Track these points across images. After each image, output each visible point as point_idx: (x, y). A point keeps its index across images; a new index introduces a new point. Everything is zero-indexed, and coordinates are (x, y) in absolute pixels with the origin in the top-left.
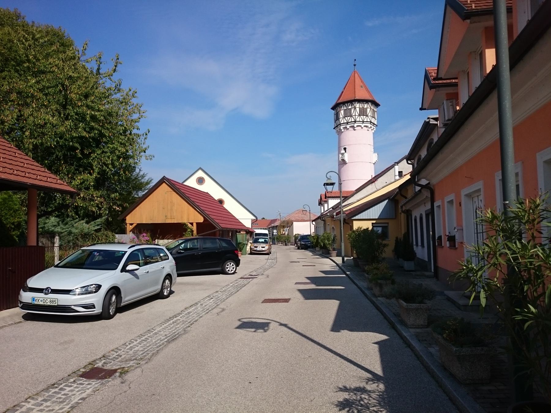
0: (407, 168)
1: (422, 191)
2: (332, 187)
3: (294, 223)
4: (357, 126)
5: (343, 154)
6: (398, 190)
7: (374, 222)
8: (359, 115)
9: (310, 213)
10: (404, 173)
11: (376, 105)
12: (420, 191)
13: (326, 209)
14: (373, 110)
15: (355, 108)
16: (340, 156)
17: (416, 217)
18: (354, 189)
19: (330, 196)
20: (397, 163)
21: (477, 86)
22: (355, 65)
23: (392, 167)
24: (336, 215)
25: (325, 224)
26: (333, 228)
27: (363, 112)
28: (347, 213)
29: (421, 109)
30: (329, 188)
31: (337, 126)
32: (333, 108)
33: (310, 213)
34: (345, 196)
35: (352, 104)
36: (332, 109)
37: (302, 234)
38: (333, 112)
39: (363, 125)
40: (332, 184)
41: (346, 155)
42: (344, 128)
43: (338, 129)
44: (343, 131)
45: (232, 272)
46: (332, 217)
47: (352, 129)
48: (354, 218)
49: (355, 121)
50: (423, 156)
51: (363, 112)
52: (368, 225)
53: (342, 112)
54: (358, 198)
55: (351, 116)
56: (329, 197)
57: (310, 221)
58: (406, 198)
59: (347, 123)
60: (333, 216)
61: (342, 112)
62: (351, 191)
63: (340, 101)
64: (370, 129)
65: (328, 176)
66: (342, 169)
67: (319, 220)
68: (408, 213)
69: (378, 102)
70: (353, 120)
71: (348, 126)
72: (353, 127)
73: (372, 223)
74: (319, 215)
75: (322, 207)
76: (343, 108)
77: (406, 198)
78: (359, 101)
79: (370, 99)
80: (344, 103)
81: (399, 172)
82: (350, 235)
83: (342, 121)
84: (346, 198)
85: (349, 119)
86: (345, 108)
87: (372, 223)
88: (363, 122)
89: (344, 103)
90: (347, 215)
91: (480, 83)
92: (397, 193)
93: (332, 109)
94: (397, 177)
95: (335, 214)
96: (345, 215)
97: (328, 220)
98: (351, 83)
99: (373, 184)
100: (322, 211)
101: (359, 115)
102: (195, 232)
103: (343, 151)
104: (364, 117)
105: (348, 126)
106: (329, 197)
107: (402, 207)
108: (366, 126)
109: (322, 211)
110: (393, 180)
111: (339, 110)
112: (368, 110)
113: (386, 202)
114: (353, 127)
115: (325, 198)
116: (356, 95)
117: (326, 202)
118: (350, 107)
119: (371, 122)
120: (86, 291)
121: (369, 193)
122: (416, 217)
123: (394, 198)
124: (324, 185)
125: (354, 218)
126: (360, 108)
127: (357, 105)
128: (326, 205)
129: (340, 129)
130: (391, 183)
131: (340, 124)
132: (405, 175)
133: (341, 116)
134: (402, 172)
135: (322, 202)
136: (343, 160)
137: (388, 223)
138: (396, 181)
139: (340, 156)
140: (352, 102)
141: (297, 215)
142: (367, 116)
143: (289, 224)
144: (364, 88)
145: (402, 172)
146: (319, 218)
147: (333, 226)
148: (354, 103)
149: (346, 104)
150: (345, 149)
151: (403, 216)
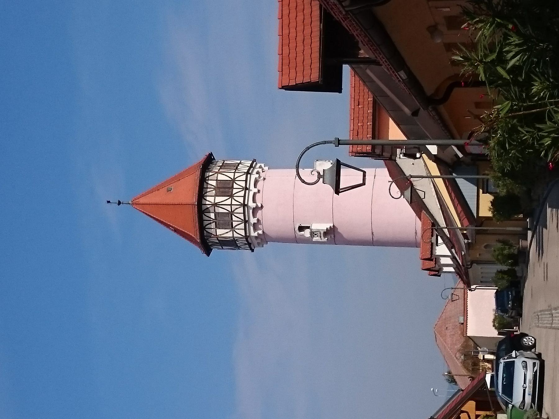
3: (469, 335)
4: (254, 201)
5: (313, 234)
7: (481, 191)
8: (231, 196)
11: (209, 161)
14: (221, 167)
15: (215, 205)
16: (316, 239)
19: (429, 253)
22: (119, 203)
24: (468, 239)
25: (479, 262)
26: (486, 247)
27: (226, 189)
31: (250, 244)
32: (208, 251)
35: (207, 210)
36: (208, 254)
37: (494, 306)
38: (215, 251)
39: (253, 190)
42: (255, 230)
43: (255, 242)
44: (260, 232)
45: (533, 339)
47: (259, 214)
49: (244, 205)
51: (226, 189)
52: (486, 200)
53: (220, 232)
55: (232, 213)
59: (246, 222)
60: (468, 243)
61: (220, 232)
64: (262, 175)
66: (345, 236)
69: (201, 157)
70: (241, 210)
71: (253, 220)
72: (255, 210)
73: (483, 193)
75: (445, 269)
76: (213, 231)
78: (201, 195)
79: (198, 173)
80: (202, 228)
82: (498, 220)
87: (483, 193)
89: (202, 228)
93: (208, 254)
95: (466, 241)
98: (158, 214)
100: (452, 269)
101: (231, 196)
102: (488, 413)
103: (307, 233)
105: (253, 220)
111: (215, 240)
112: (221, 177)
114: (255, 210)
115: (432, 260)
118: (212, 216)
119: (248, 173)
120: (525, 367)
126: (216, 195)
127: (210, 200)
128: (443, 261)
129: (256, 237)
131: (247, 237)
133: (230, 235)
135: (437, 268)
139: (316, 239)
140: (201, 211)
141: (449, 340)
142: (234, 180)
143: (470, 348)
144: (172, 186)
148: (204, 207)
149: (206, 223)
150: (301, 229)
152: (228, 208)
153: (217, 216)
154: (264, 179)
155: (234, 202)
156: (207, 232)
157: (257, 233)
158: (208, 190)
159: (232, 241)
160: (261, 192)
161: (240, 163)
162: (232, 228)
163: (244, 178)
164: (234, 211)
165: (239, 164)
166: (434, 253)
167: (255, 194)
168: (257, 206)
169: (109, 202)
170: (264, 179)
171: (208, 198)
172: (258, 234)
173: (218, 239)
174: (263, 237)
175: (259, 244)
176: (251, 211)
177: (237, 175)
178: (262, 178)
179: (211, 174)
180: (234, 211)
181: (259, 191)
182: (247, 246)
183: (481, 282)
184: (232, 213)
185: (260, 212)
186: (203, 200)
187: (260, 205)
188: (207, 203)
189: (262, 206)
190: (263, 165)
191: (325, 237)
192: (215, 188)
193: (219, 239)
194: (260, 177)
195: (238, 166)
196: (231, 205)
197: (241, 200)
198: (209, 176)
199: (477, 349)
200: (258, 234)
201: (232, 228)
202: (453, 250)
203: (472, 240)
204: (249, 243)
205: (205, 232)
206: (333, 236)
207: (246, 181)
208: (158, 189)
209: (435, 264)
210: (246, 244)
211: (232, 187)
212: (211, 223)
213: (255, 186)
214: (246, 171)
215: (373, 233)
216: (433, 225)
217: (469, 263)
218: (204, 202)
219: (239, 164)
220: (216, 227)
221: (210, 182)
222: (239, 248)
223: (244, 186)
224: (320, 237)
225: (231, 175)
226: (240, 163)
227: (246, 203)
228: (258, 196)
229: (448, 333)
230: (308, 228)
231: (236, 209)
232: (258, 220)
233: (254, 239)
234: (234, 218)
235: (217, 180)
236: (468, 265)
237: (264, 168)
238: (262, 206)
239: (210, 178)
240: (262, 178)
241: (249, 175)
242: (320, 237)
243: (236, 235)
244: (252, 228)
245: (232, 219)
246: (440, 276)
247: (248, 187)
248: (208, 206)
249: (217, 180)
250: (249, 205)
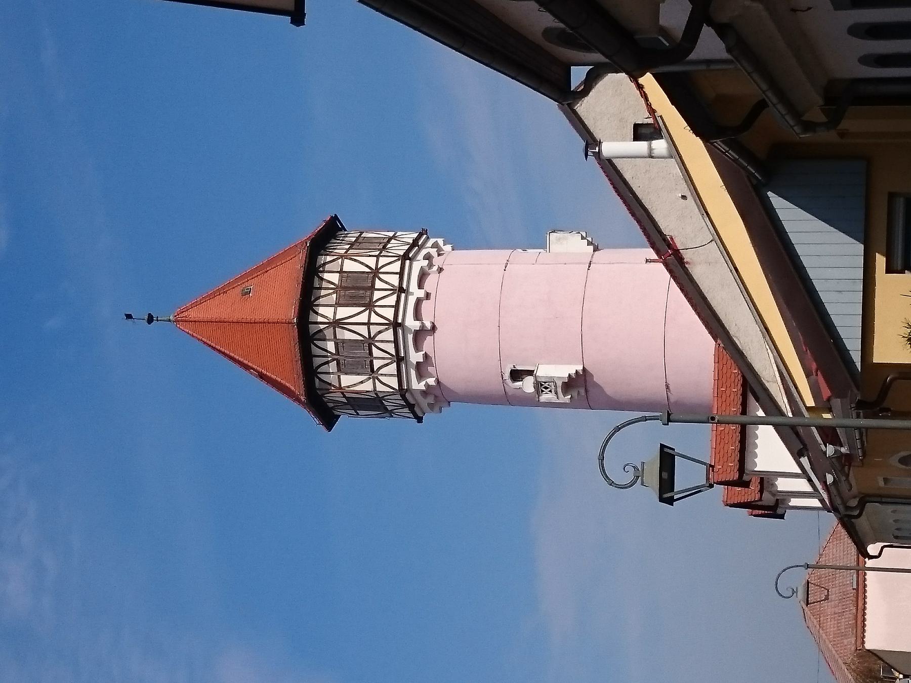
0: (617, 101)
1: (724, 17)
2: (691, 447)
4: (417, 316)
5: (540, 386)
6: (718, 143)
7: (881, 261)
8: (370, 306)
9: (817, 567)
10: (643, 117)
11: (331, 230)
12: (722, 30)
13: (803, 485)
14: (352, 245)
15: (337, 323)
16: (546, 397)
17: (866, 60)
18: (707, 343)
19: (733, 464)
20: (591, 142)
21: (551, 18)
22: (150, 319)
23: (609, 167)
24: (836, 442)
25: (883, 498)
27: (359, 291)
28: (826, 392)
29: (298, 18)
30: (686, 475)
31: (411, 407)
32: (328, 418)
33: (817, 567)
34: (737, 389)
38: (345, 421)
39: (416, 293)
40: (667, 459)
41: (544, 371)
43: (424, 402)
44: (431, 381)
46: (843, 463)
47: (428, 344)
48: (856, 357)
49: (396, 325)
50: (547, 20)
51: (359, 291)
53: (347, 380)
54: (755, 330)
55: (370, 341)
56: (742, 469)
57: (861, 571)
58: (761, 105)
59: (400, 360)
60: (839, 456)
61: (347, 380)
62: (718, 360)
63: (299, 389)
65: (630, 477)
66: (609, 391)
67: (862, 523)
68: (843, 96)
69: (316, 225)
70: (389, 335)
71: (415, 357)
72: (419, 336)
73: (888, 271)
74: (831, 520)
75: (794, 502)
76: (332, 379)
77: (761, 105)
80: (310, 372)
81: (637, 137)
84: (751, 386)
86: (333, 367)
87: (888, 271)
88: (401, 290)
89: (310, 372)
90: (837, 392)
91: (548, 14)
92: (731, 144)
94: (660, 146)
95: (830, 450)
96: (837, 403)
97: (857, 481)
98: (227, 340)
99: (687, 256)
101: (370, 306)
103: (528, 385)
104: (378, 284)
105: (415, 357)
106: (742, 469)
107: (809, 126)
109: (815, 503)
110: (673, 166)
113: (776, 201)
114: (419, 336)
115: (746, 485)
116: (281, 317)
117: (766, 480)
118: (331, 346)
119: (405, 257)
121: (730, 277)
122: (866, 60)
123: (762, 164)
124: (670, 501)
125: (856, 357)
127: (326, 312)
128: (783, 485)
129: (424, 393)
130: (686, 178)
131: (403, 392)
132: (652, 111)
133: (368, 386)
134: (636, 126)
136: (570, 384)
137: (892, 196)
138: (675, 152)
139: (546, 397)
140: (306, 336)
142: (376, 273)
144: (252, 284)
145: (636, 126)
146: (848, 523)
147: (894, 461)
148: (313, 329)
149: (317, 361)
150: (517, 375)
151: (859, 123)
152: (363, 330)
153: (341, 349)
154: (440, 270)
155: (375, 319)
156: (320, 379)
157: (423, 383)
158: (323, 292)
159: (374, 399)
160: (432, 297)
161: (394, 237)
162: (373, 373)
163: (396, 267)
164: (375, 336)
165: (390, 239)
166: (748, 466)
167: (419, 302)
168: (423, 325)
169: (129, 316)
170: (440, 270)
171: (321, 310)
172: (427, 385)
173: (344, 396)
174: (438, 393)
175: (431, 406)
176: (410, 337)
177: (383, 260)
178: (435, 268)
179: (329, 258)
180: (375, 336)
181: (428, 296)
182: (406, 410)
183: (896, 537)
184: (370, 341)
185: (429, 339)
186: (311, 312)
187: (428, 325)
188: (320, 319)
189: (434, 328)
190: (440, 241)
191: (565, 393)
192: (338, 289)
193: (347, 395)
194: (431, 265)
195: (389, 242)
196: (369, 324)
197: (389, 313)
198: (325, 264)
199: (893, 674)
200: (427, 385)
201: (373, 373)
202: (805, 461)
203: (850, 448)
204: (410, 404)
205: (317, 381)
206: (582, 391)
207: (401, 274)
208: (223, 291)
209: (761, 491)
210: (403, 407)
211: (372, 288)
212: (327, 363)
213: (420, 286)
214: (401, 253)
215: (667, 387)
216: (745, 384)
217: (854, 503)
218: (313, 317)
219: (390, 239)
220: (339, 370)
221: (326, 276)
222: (391, 413)
223: (396, 284)
224: (556, 393)
225: (371, 262)
226: (394, 237)
227: (400, 321)
228: (425, 305)
229: (828, 608)
230: (530, 373)
231: (380, 332)
232: (426, 356)
233: (420, 398)
234: (376, 352)
235: (341, 272)
236: (848, 508)
237: (444, 248)
238: (434, 328)
239: (327, 267)
240: (435, 268)
241: (408, 262)
242: (556, 393)
243: (380, 388)
244: (413, 373)
245: (371, 353)
246: (782, 517)
248: (322, 326)
249: (341, 272)
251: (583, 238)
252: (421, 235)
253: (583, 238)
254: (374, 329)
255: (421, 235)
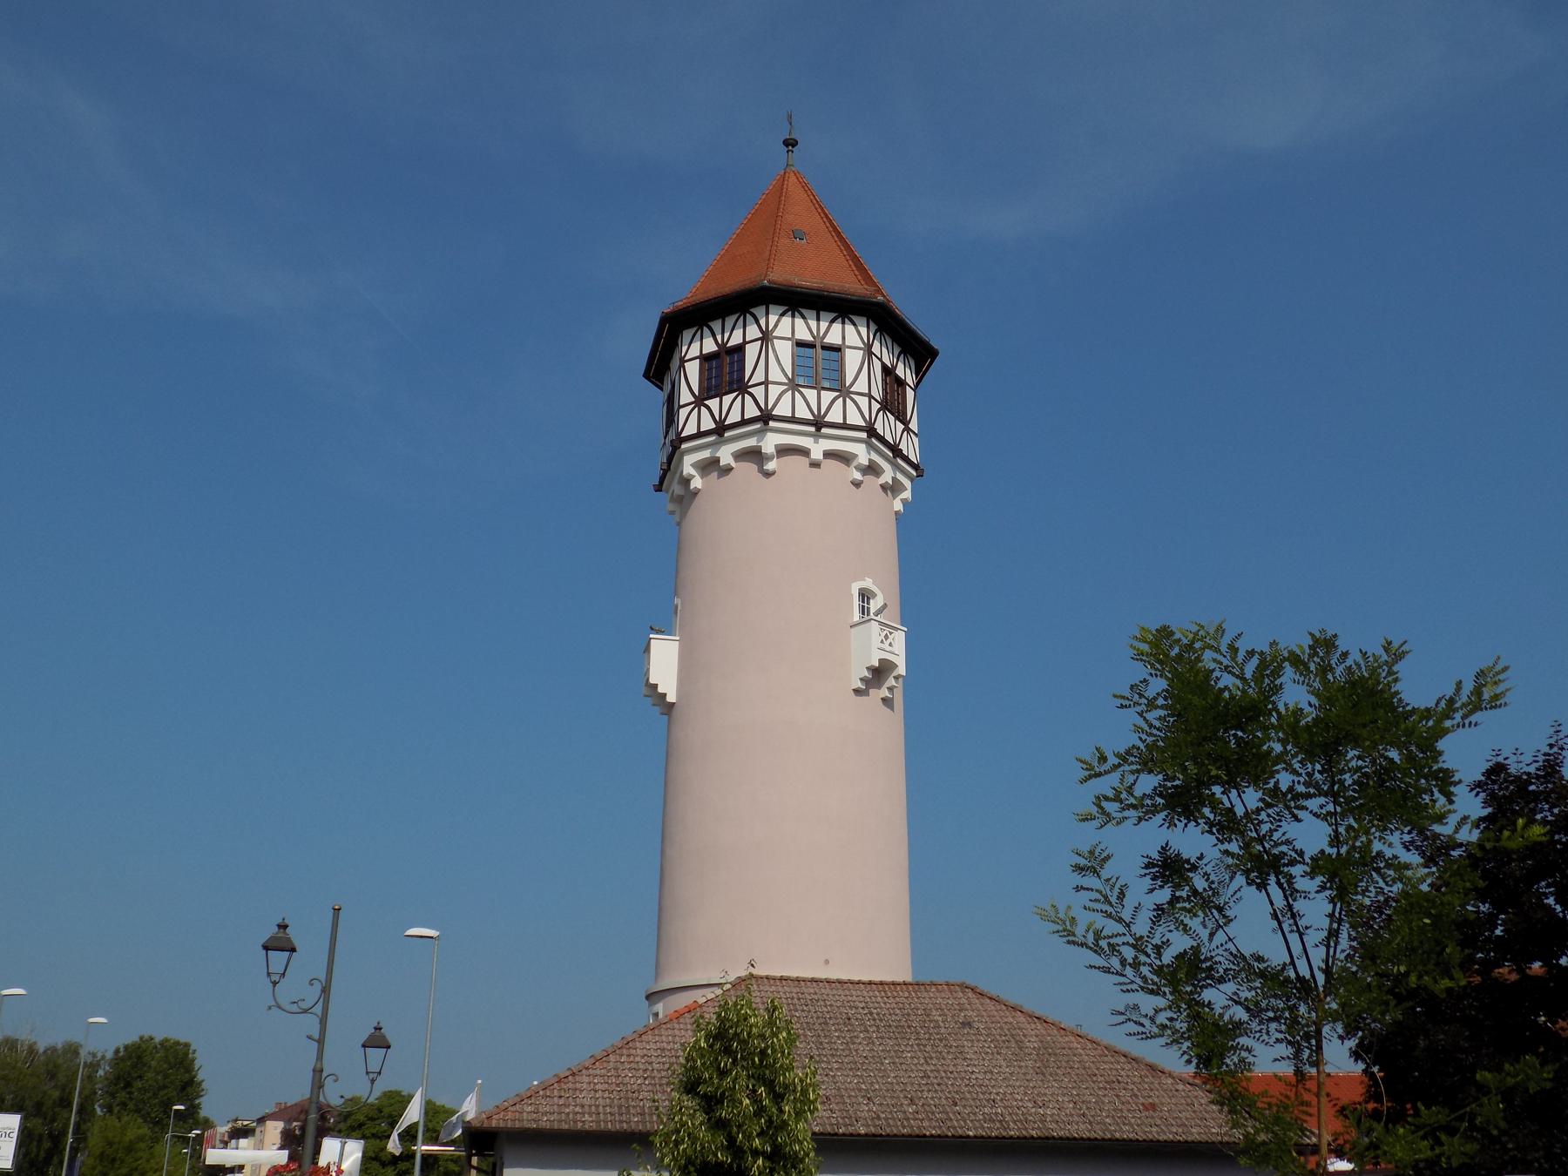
4: (784, 451)
8: (793, 386)
11: (919, 352)
15: (766, 338)
22: (790, 143)
27: (818, 366)
39: (817, 449)
44: (697, 483)
47: (750, 468)
49: (766, 417)
51: (818, 366)
70: (752, 411)
71: (726, 455)
72: (755, 455)
78: (796, 301)
83: (690, 422)
85: (733, 407)
98: (769, 216)
104: (827, 396)
105: (726, 455)
108: (845, 458)
114: (755, 455)
119: (871, 431)
127: (789, 328)
133: (685, 397)
140: (743, 303)
142: (844, 391)
152: (759, 377)
155: (774, 391)
157: (693, 472)
158: (813, 324)
161: (907, 429)
163: (855, 418)
165: (906, 423)
167: (805, 452)
168: (770, 458)
177: (863, 402)
181: (815, 465)
187: (771, 466)
197: (783, 409)
213: (829, 455)
226: (907, 429)
227: (772, 424)
232: (729, 469)
238: (768, 474)
244: (706, 454)
247: (824, 430)
248: (763, 322)
250: (770, 435)
251: (1331, 916)
252: (915, 467)
253: (1331, 916)
254: (758, 392)
255: (915, 467)
